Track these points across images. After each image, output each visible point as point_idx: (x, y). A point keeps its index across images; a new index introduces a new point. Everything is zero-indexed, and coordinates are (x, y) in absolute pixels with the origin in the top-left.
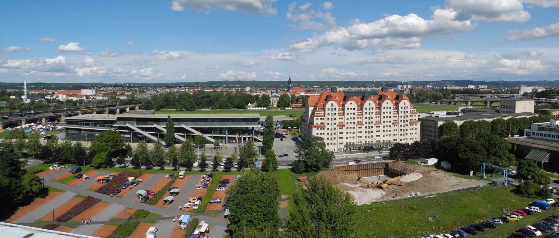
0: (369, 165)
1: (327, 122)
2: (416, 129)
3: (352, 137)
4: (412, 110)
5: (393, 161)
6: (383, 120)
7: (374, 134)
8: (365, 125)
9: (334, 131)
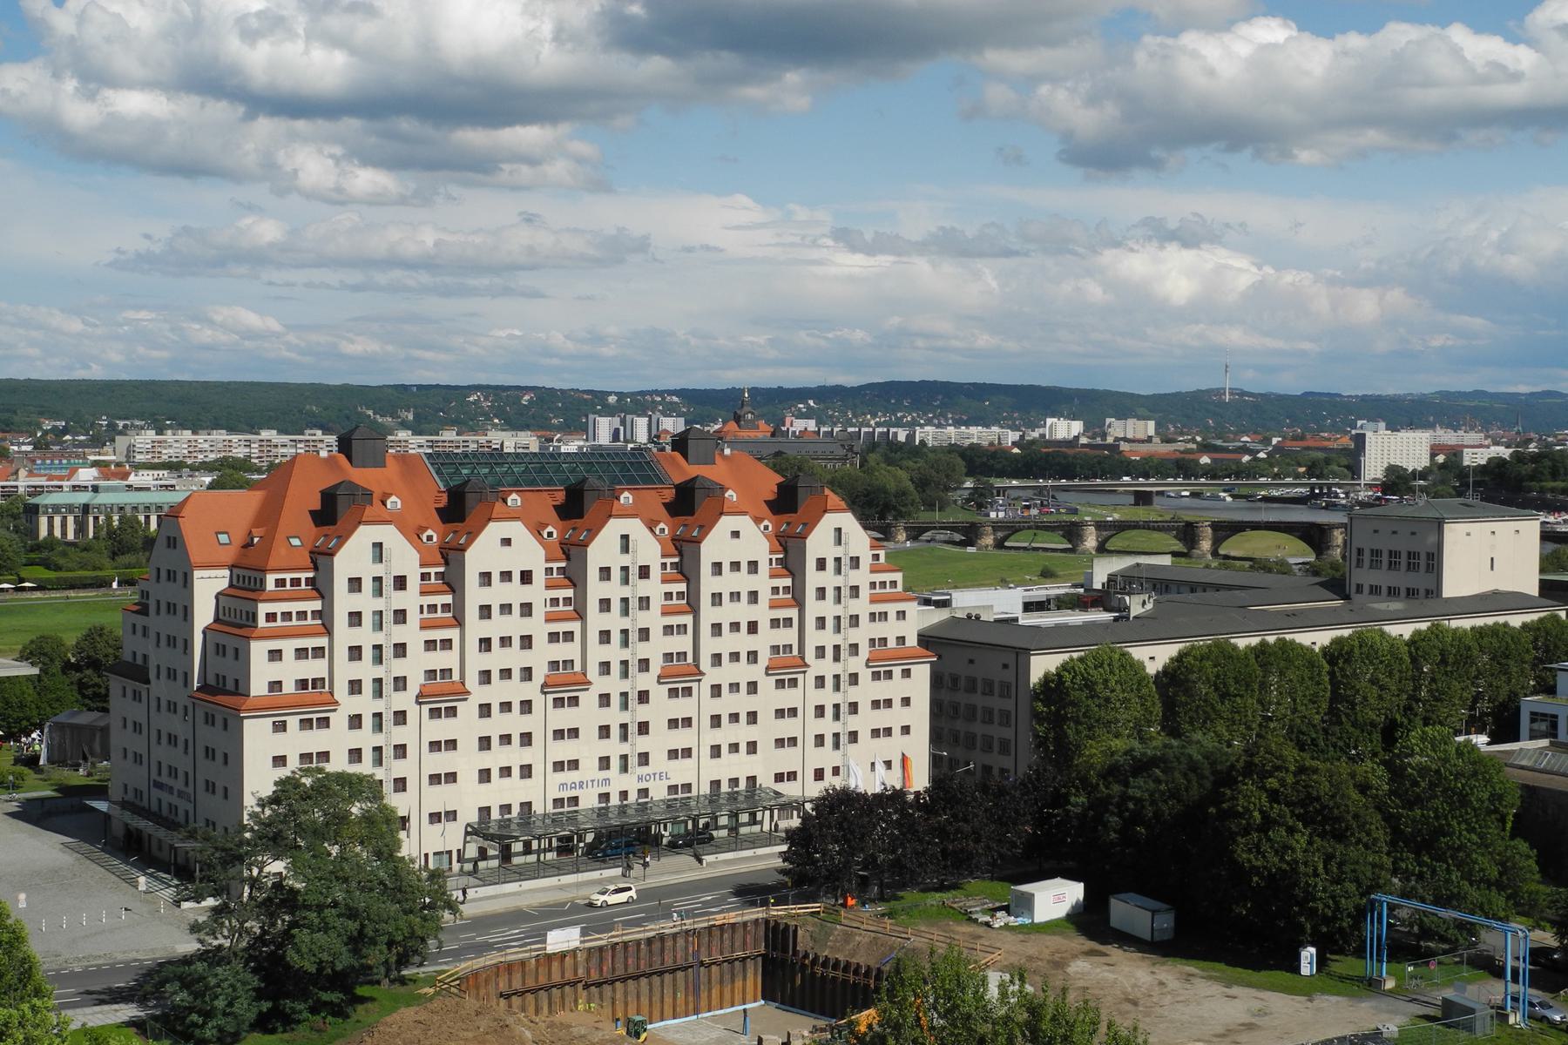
0: (669, 944)
1: (346, 671)
2: (906, 701)
3: (516, 772)
4: (879, 577)
5: (815, 907)
6: (709, 645)
7: (659, 742)
8: (600, 684)
9: (399, 735)
